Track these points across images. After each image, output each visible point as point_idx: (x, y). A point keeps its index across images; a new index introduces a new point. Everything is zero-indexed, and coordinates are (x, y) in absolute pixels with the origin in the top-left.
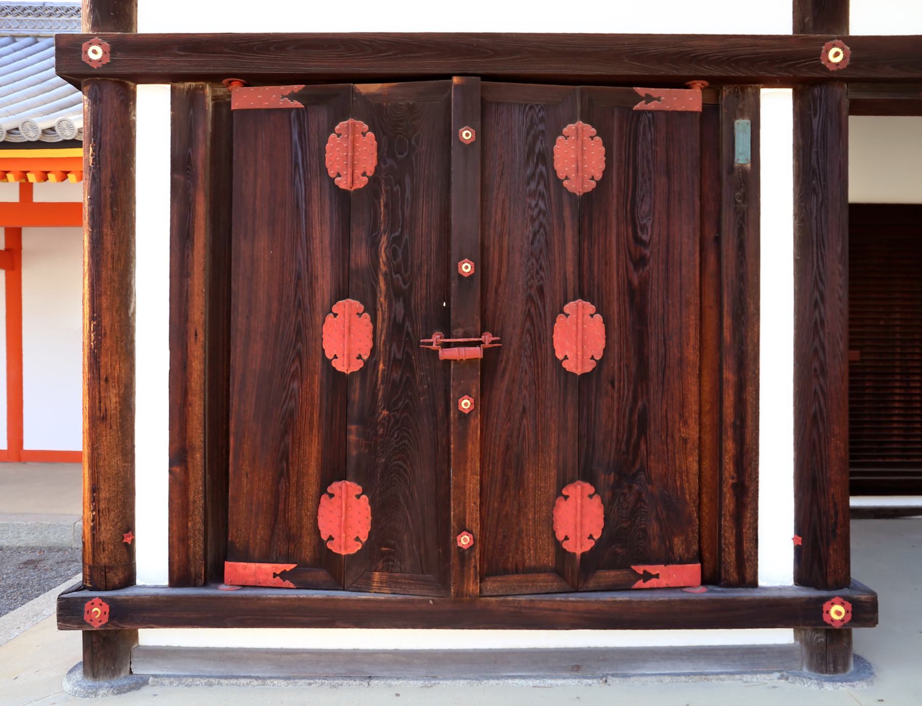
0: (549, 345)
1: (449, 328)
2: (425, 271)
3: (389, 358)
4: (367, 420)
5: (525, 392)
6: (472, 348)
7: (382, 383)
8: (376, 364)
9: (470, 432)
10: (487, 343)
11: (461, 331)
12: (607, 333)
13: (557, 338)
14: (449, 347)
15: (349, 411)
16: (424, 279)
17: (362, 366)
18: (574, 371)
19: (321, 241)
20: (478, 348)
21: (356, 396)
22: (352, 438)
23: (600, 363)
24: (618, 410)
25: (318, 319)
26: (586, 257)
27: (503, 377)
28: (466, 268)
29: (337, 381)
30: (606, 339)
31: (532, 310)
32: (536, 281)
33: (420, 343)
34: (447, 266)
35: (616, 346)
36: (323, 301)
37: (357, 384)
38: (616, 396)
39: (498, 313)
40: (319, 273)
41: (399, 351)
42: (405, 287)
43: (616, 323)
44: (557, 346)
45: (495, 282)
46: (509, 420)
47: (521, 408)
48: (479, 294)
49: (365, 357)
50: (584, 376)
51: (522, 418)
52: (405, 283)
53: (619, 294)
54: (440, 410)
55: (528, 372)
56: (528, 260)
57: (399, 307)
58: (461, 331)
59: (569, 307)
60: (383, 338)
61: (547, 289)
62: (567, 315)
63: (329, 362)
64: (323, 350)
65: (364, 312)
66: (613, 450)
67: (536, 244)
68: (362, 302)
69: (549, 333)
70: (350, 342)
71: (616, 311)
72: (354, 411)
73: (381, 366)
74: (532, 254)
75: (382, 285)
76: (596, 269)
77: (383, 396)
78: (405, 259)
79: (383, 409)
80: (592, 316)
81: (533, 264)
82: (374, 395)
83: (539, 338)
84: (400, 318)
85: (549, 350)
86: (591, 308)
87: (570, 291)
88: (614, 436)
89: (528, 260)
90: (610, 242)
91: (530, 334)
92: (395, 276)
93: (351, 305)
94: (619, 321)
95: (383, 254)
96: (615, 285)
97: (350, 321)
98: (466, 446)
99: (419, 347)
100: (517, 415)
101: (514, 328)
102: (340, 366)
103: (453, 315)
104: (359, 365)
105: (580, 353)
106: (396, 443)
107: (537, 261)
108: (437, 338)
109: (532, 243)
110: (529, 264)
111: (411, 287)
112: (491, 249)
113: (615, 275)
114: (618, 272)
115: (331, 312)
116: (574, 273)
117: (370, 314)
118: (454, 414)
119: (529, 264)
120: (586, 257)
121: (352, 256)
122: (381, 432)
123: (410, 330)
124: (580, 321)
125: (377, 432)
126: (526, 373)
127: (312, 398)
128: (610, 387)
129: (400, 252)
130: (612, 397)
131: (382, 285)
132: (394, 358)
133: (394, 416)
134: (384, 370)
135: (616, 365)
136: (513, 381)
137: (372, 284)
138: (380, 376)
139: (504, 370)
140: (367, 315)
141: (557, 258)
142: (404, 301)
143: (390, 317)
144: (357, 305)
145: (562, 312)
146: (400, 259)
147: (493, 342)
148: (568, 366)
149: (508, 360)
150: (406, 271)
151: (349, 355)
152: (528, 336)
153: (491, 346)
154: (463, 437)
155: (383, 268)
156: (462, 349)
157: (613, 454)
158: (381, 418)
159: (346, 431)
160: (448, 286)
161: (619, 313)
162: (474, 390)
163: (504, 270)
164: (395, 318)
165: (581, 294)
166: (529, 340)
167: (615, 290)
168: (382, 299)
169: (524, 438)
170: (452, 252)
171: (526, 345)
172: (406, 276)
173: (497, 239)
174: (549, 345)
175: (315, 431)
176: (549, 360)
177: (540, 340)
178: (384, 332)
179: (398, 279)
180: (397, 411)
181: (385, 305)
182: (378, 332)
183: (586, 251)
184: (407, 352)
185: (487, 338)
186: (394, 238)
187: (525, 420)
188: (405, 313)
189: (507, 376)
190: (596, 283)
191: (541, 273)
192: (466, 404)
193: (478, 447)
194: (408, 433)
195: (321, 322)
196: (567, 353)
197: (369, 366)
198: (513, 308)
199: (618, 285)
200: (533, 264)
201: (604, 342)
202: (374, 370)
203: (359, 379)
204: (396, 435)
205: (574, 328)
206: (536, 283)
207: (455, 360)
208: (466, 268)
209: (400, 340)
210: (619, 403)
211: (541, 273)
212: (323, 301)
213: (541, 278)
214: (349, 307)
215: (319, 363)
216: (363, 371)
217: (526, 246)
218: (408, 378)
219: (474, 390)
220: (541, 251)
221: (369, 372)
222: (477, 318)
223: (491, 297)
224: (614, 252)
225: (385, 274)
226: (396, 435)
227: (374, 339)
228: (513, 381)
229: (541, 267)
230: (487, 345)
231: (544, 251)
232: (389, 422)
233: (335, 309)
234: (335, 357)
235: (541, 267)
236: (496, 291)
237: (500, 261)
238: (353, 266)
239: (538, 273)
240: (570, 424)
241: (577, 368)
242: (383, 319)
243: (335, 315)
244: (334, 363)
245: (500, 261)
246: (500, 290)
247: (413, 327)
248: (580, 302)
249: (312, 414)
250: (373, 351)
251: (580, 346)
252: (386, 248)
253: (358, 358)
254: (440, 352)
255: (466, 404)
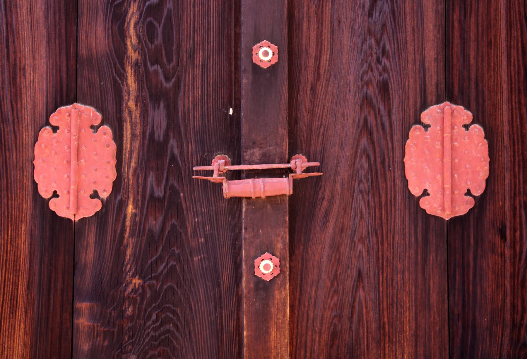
0: (398, 173)
1: (239, 148)
2: (199, 59)
3: (144, 196)
4: (107, 293)
5: (360, 247)
6: (275, 180)
7: (132, 235)
8: (122, 205)
9: (274, 310)
10: (299, 171)
11: (257, 153)
12: (491, 154)
13: (411, 162)
14: (239, 178)
15: (78, 280)
16: (198, 72)
17: (99, 208)
18: (438, 213)
19: (31, 11)
20: (285, 179)
21: (89, 255)
22: (83, 322)
23: (481, 202)
24: (513, 276)
25: (27, 136)
26: (457, 34)
27: (325, 223)
28: (265, 54)
29: (57, 232)
30: (490, 163)
31: (371, 120)
32: (376, 74)
33: (192, 172)
34: (234, 52)
35: (507, 175)
36: (35, 106)
37: (91, 237)
38: (508, 253)
39: (316, 124)
40: (29, 62)
41: (158, 185)
42: (168, 85)
43: (506, 137)
44: (410, 175)
45: (311, 78)
46: (336, 292)
47: (355, 274)
48: (286, 94)
49: (104, 195)
50: (455, 220)
51: (356, 289)
52: (168, 79)
53: (511, 91)
54: (226, 277)
55: (366, 216)
56: (364, 41)
57: (159, 117)
58: (257, 153)
59: (430, 115)
60: (133, 164)
61: (393, 86)
62: (426, 127)
63: (45, 203)
64: (35, 185)
65: (102, 124)
66: (506, 340)
67: (376, 15)
68: (100, 109)
69: (398, 154)
70: (79, 171)
71: (506, 118)
72: (86, 281)
73: (130, 209)
74: (369, 32)
75: (131, 82)
76: (472, 53)
77: (134, 255)
78: (168, 39)
79: (133, 276)
80: (467, 127)
81: (371, 48)
82: (119, 254)
83: (383, 162)
84: (160, 134)
85: (398, 182)
86: (464, 115)
87: (431, 88)
88: (508, 316)
89: (364, 41)
90: (496, 10)
91: (368, 157)
92: (152, 69)
93: (80, 114)
94: (511, 135)
95: (132, 32)
96: (505, 78)
97: (79, 139)
98: (267, 333)
99: (191, 180)
100: (349, 283)
101: (342, 146)
102: (62, 208)
103: (245, 128)
104: (96, 206)
105: (447, 186)
106: (155, 329)
107: (378, 42)
108: (219, 164)
109: (370, 15)
110: (366, 47)
111: (177, 86)
112: (305, 25)
113: (504, 62)
114: (509, 56)
115: (48, 123)
116: (436, 59)
117: (111, 127)
118: (248, 283)
119: (366, 47)
120: (457, 34)
121: (82, 36)
122: (129, 311)
123: (176, 151)
124: (447, 135)
125: (123, 312)
126: (361, 218)
127: (16, 260)
128: (498, 239)
129: (160, 30)
130: (503, 254)
131: (131, 82)
132: (152, 196)
133: (151, 287)
134: (134, 215)
135: (507, 204)
136: (342, 230)
137: (115, 81)
138: (128, 223)
139: (327, 213)
140: (106, 129)
141: (410, 38)
142: (167, 107)
143: (144, 133)
144: (90, 113)
145: (418, 121)
146: (159, 40)
147: (308, 170)
148: (429, 205)
149: (333, 197)
150: (169, 61)
151: (78, 191)
152: (364, 159)
153: (305, 175)
154: (263, 318)
155: (132, 55)
156: (260, 181)
157: (505, 347)
158: (129, 289)
159: (73, 312)
160: (237, 82)
161: (511, 123)
162: (279, 245)
163: (325, 58)
164: (152, 133)
165: (449, 94)
166: (366, 166)
167: (505, 86)
168: (132, 104)
169: (360, 320)
170: (243, 29)
171: (362, 173)
172: (170, 67)
173: (313, 8)
174: (398, 173)
175: (20, 313)
176: (399, 197)
177: (384, 165)
178: (135, 155)
179: (156, 72)
180: (156, 278)
181: (136, 113)
182: (126, 155)
183: (456, 24)
184: (172, 187)
185: (300, 163)
186: (150, 7)
187: (361, 293)
188: (168, 126)
189: (331, 223)
190: (473, 75)
191: (384, 61)
192: (266, 267)
193: (287, 333)
194: (174, 312)
195: (31, 140)
196: (427, 186)
197: (112, 208)
198: (341, 118)
199: (510, 78)
200: (371, 48)
201: (487, 168)
202: (117, 219)
203: (93, 228)
204: (154, 317)
205: (438, 147)
206: (376, 77)
207: (249, 198)
208: (265, 54)
209: (160, 168)
210: (513, 264)
211: (384, 61)
212: (35, 106)
213: (385, 69)
214: (77, 117)
215: (28, 205)
216: (100, 217)
217: (360, 20)
218: (173, 226)
219: (279, 245)
220: (384, 25)
221: (111, 218)
222: (283, 132)
223: (305, 99)
224: (503, 25)
225: (137, 64)
226: (154, 317)
227: (119, 167)
228: (342, 230)
229: (384, 52)
230: (299, 174)
231: (388, 25)
232: (143, 295)
233: (54, 119)
234: (55, 195)
235: (384, 52)
236: (313, 89)
237: (320, 43)
238: (83, 51)
239: (379, 61)
240: (434, 297)
241: (443, 210)
242: (133, 135)
243: (55, 129)
244: (53, 205)
245: (320, 43)
246: (320, 88)
247: (181, 146)
248: (447, 106)
249: (16, 285)
250: (117, 185)
251: (447, 174)
252: (136, 24)
253: (92, 197)
254: (225, 186)
255: (266, 267)
